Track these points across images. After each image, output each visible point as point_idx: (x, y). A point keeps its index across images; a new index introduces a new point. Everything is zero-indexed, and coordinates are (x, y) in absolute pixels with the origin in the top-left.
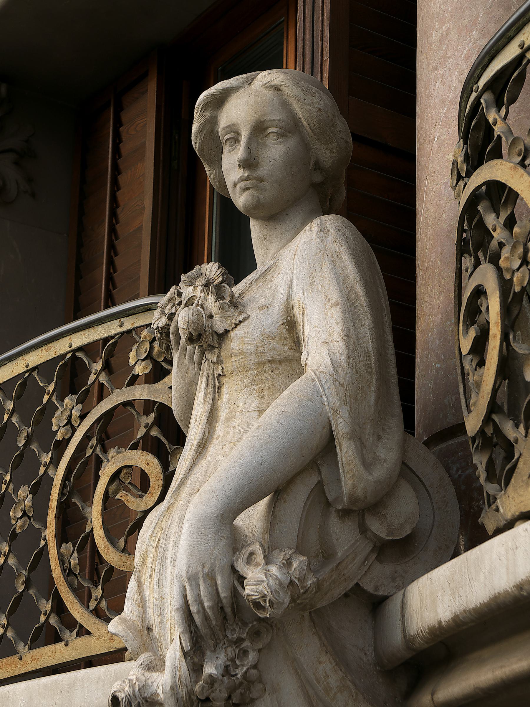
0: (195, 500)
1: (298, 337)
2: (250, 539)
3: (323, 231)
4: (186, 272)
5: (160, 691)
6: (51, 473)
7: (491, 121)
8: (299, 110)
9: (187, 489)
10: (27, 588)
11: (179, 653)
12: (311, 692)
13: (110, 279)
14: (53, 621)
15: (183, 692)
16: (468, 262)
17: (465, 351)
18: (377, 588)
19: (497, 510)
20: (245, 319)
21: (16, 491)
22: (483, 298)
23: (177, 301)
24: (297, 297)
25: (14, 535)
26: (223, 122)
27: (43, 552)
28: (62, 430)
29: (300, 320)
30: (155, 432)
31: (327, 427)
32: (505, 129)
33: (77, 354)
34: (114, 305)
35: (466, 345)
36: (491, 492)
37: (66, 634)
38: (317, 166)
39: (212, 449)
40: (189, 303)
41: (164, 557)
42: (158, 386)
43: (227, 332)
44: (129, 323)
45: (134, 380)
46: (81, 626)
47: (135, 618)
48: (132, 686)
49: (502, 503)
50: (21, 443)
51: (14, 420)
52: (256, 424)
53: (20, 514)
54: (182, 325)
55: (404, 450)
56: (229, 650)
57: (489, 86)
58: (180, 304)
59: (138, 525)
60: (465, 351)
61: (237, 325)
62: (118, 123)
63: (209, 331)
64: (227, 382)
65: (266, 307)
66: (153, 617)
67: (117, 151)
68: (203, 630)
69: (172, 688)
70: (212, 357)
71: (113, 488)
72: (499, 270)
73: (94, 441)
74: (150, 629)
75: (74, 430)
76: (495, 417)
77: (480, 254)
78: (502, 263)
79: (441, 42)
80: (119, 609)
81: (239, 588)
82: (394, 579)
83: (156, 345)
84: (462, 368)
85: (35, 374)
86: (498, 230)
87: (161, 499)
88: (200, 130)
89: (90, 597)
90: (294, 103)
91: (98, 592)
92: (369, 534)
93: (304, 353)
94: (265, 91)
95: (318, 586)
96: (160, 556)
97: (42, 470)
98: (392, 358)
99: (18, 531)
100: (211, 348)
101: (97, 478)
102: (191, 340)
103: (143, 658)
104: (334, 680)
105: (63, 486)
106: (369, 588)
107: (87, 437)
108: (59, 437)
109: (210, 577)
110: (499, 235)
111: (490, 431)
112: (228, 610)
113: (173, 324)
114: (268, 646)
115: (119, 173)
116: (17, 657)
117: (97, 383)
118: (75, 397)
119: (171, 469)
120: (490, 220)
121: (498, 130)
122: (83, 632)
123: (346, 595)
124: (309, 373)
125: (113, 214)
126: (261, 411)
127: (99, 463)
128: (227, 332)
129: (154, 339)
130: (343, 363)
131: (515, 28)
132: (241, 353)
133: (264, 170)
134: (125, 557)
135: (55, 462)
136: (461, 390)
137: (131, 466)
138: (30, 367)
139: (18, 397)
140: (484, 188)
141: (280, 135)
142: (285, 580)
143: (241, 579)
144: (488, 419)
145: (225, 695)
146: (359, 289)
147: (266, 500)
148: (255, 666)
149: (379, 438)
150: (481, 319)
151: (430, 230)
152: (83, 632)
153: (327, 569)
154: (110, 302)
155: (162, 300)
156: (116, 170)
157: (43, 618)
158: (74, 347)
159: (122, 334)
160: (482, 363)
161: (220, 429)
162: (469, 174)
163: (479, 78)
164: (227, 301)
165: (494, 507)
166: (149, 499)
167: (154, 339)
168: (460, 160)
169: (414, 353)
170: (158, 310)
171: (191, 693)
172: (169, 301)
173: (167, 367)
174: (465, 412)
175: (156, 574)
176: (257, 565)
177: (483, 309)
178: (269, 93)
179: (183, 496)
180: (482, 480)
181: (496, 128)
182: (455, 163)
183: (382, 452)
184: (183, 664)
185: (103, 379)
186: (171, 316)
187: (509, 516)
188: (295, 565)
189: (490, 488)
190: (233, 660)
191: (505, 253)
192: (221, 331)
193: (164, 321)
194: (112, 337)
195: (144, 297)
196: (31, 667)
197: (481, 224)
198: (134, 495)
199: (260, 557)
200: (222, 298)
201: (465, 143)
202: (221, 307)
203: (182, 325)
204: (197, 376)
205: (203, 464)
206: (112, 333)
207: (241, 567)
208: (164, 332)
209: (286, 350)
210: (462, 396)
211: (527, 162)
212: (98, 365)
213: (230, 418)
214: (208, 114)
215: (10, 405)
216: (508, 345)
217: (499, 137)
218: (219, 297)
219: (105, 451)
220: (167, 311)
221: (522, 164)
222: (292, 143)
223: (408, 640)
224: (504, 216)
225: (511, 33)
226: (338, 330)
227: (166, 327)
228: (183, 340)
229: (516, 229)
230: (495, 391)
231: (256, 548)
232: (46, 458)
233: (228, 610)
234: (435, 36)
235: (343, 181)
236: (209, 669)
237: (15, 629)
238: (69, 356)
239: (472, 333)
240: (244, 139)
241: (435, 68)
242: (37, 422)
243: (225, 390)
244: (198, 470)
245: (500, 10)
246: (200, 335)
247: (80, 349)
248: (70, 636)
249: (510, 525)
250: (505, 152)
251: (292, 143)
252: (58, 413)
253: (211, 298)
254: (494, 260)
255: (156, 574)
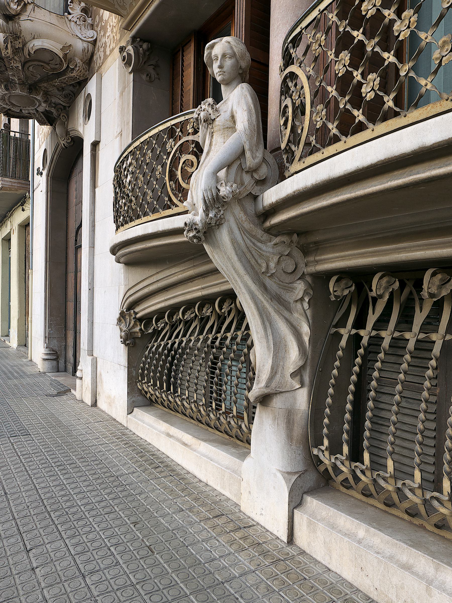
0: (206, 168)
1: (235, 121)
2: (221, 179)
3: (243, 88)
4: (203, 101)
5: (197, 221)
6: (166, 161)
7: (291, 53)
8: (235, 50)
9: (204, 165)
10: (161, 194)
11: (202, 211)
12: (238, 221)
13: (181, 105)
14: (169, 203)
15: (203, 221)
16: (283, 97)
17: (281, 125)
18: (256, 193)
19: (289, 171)
20: (220, 115)
21: (157, 167)
22: (287, 108)
23: (200, 110)
24: (235, 108)
25: (157, 179)
26: (213, 54)
27: (165, 184)
28: (169, 149)
29: (235, 116)
30: (195, 149)
31: (242, 148)
32: (295, 55)
33: (173, 126)
34: (183, 112)
35: (282, 122)
36: (288, 166)
37: (172, 207)
38: (241, 68)
39: (211, 154)
40: (204, 110)
41: (198, 185)
42: (195, 136)
43: (215, 119)
44: (187, 117)
45: (189, 134)
46: (176, 204)
47: (190, 202)
48: (190, 220)
49: (290, 169)
50: (158, 153)
51: (157, 207)
52: (223, 146)
53: (158, 173)
54: (202, 117)
55: (264, 154)
56: (216, 210)
57: (291, 41)
58: (201, 111)
59: (191, 176)
60: (281, 125)
61: (217, 117)
62: (183, 56)
63: (210, 119)
64: (214, 134)
65: (226, 111)
66: (195, 201)
67: (183, 65)
68: (209, 205)
69: (201, 220)
70: (210, 126)
71: (183, 166)
72: (292, 99)
73: (178, 152)
74: (194, 205)
75: (172, 149)
76: (289, 144)
77: (287, 95)
78: (293, 98)
79: (277, 28)
80: (186, 200)
81: (219, 193)
82: (260, 191)
83: (195, 124)
84: (281, 130)
85: (161, 132)
86: (292, 87)
87: (197, 169)
88: (207, 56)
89: (178, 196)
90: (234, 47)
91: (180, 195)
92: (254, 178)
93: (236, 125)
94: (225, 43)
95: (240, 192)
96: (197, 184)
97: (164, 160)
98: (261, 127)
99: (158, 178)
100: (210, 124)
101: (179, 163)
102: (204, 121)
103: (193, 212)
104: (244, 218)
105: (170, 165)
106: (254, 193)
107: (176, 151)
108: (168, 151)
109: (211, 190)
110: (292, 89)
111: (288, 148)
112: (215, 199)
113: (199, 117)
114: (226, 209)
115: (184, 72)
116: (159, 213)
117: (178, 135)
118: (172, 139)
119: (199, 160)
120: (290, 84)
121: (293, 55)
122: (176, 206)
123: (247, 195)
124: (238, 131)
125: (182, 85)
126: (224, 143)
127: (180, 158)
128: (215, 119)
129: (194, 122)
130: (247, 128)
131: (299, 22)
132: (219, 125)
133: (225, 69)
134: (187, 185)
135: (168, 158)
136: (280, 136)
137: (188, 159)
138: (160, 130)
139: (157, 140)
140: (289, 74)
141: (230, 58)
142: (231, 191)
143: (219, 190)
144: (287, 145)
145: (215, 222)
146: (252, 106)
147: (226, 168)
148: (223, 215)
149: (257, 150)
150: (286, 115)
151: (273, 89)
152: (176, 206)
153: (242, 188)
154: (182, 111)
155: (196, 110)
156: (183, 71)
157: (166, 202)
158: (172, 124)
159: (185, 120)
160: (286, 128)
161: (213, 148)
162: (284, 70)
163: (288, 39)
164: (215, 110)
165: (288, 170)
166: (194, 169)
167: (194, 122)
168: (282, 65)
169: (267, 134)
170: (195, 112)
171: (206, 222)
172: (198, 110)
173: (198, 130)
174: (281, 143)
175: (196, 190)
176: (223, 186)
177: (287, 112)
178: (227, 44)
179: (203, 167)
180: (285, 162)
181: (293, 55)
182: (280, 66)
183: (258, 155)
184: (204, 214)
185: (180, 134)
186: (199, 114)
187: (292, 173)
188: (233, 186)
189: (287, 165)
190: (217, 213)
191: (294, 94)
192: (213, 119)
193: (197, 116)
194: (182, 121)
195: (191, 109)
196: (163, 216)
197: (287, 85)
198: (189, 168)
199: (224, 184)
200: (213, 109)
201: (283, 60)
202: (213, 111)
203: (202, 117)
204: (206, 132)
205: (208, 158)
206: (182, 120)
207: (219, 187)
208: (197, 119)
209: (231, 124)
210: (280, 138)
211: (301, 66)
212: (179, 130)
213: (215, 145)
214: (209, 51)
215: (154, 142)
216: (294, 122)
217: (293, 58)
218: (213, 108)
219: (181, 155)
220: (198, 113)
221: (300, 66)
222: (233, 60)
223: (264, 207)
224: (294, 83)
225: (298, 24)
226: (246, 118)
227: (198, 118)
228: (202, 121)
229: (297, 87)
230: (290, 136)
231: (223, 182)
232: (165, 157)
233: (215, 199)
234: (276, 26)
235: (248, 73)
236: (211, 215)
237: (157, 145)
238: (170, 127)
239: (284, 119)
240: (219, 59)
241: (275, 37)
242: (162, 147)
243: (214, 136)
244: (207, 160)
245: (295, 17)
246: (207, 120)
247: (174, 125)
248: (173, 207)
249: (292, 175)
250: (295, 64)
251: (233, 60)
252: (168, 144)
253: (210, 109)
254: (291, 96)
255: (196, 190)
